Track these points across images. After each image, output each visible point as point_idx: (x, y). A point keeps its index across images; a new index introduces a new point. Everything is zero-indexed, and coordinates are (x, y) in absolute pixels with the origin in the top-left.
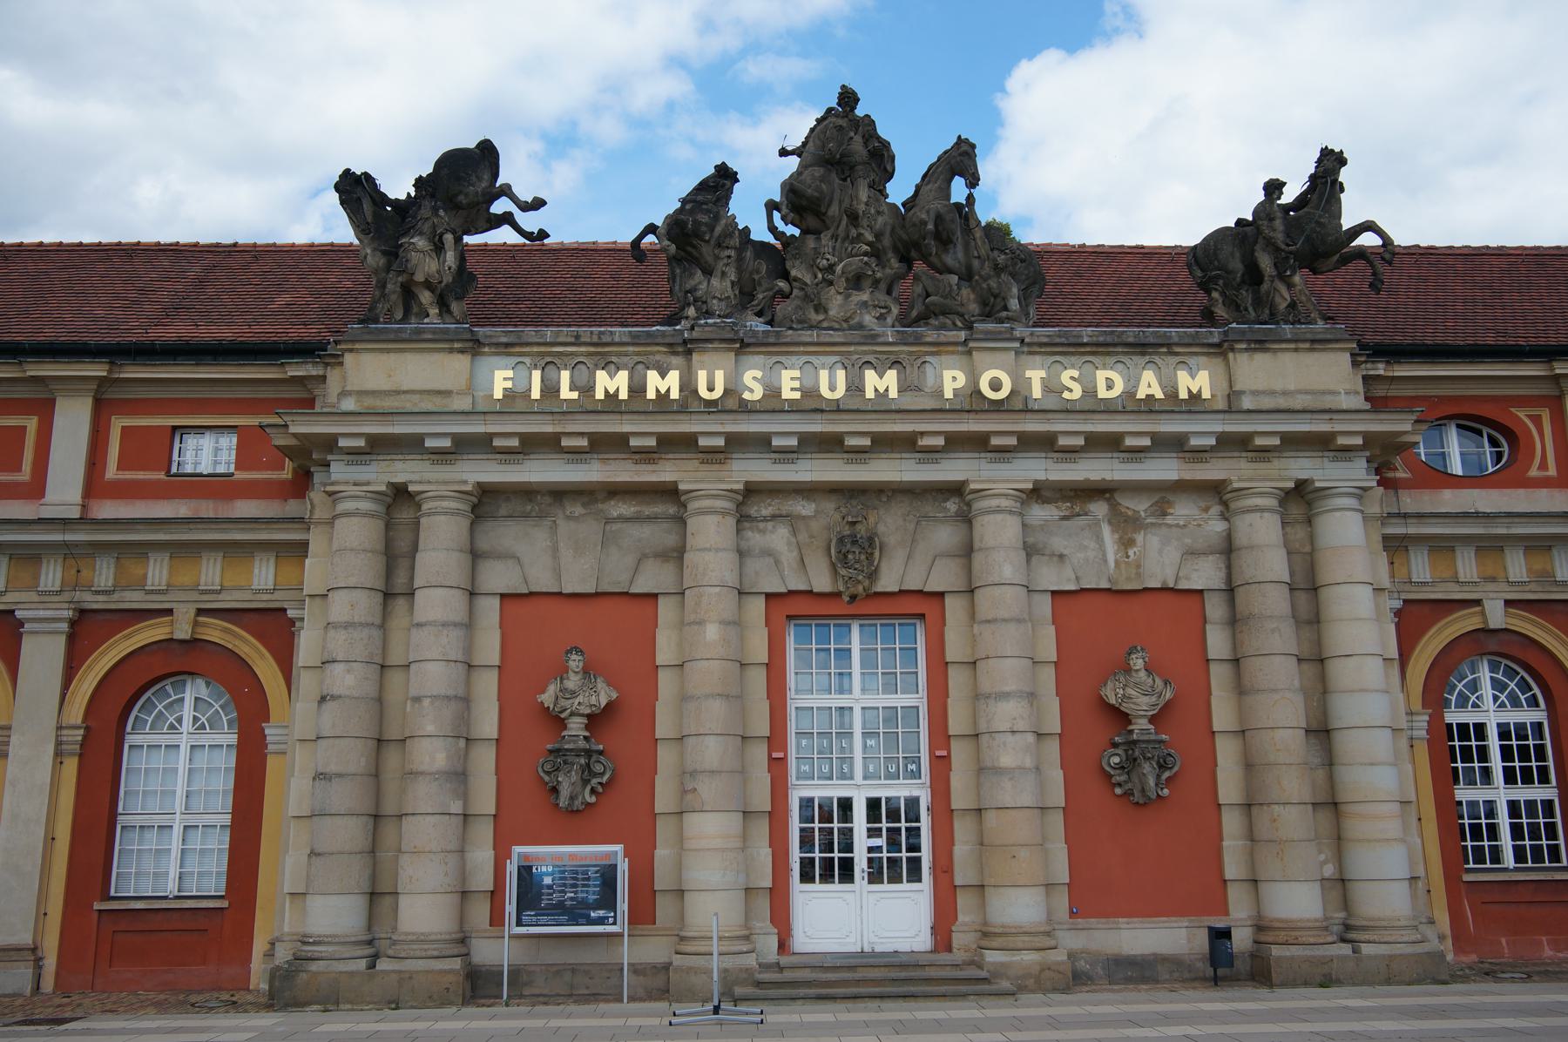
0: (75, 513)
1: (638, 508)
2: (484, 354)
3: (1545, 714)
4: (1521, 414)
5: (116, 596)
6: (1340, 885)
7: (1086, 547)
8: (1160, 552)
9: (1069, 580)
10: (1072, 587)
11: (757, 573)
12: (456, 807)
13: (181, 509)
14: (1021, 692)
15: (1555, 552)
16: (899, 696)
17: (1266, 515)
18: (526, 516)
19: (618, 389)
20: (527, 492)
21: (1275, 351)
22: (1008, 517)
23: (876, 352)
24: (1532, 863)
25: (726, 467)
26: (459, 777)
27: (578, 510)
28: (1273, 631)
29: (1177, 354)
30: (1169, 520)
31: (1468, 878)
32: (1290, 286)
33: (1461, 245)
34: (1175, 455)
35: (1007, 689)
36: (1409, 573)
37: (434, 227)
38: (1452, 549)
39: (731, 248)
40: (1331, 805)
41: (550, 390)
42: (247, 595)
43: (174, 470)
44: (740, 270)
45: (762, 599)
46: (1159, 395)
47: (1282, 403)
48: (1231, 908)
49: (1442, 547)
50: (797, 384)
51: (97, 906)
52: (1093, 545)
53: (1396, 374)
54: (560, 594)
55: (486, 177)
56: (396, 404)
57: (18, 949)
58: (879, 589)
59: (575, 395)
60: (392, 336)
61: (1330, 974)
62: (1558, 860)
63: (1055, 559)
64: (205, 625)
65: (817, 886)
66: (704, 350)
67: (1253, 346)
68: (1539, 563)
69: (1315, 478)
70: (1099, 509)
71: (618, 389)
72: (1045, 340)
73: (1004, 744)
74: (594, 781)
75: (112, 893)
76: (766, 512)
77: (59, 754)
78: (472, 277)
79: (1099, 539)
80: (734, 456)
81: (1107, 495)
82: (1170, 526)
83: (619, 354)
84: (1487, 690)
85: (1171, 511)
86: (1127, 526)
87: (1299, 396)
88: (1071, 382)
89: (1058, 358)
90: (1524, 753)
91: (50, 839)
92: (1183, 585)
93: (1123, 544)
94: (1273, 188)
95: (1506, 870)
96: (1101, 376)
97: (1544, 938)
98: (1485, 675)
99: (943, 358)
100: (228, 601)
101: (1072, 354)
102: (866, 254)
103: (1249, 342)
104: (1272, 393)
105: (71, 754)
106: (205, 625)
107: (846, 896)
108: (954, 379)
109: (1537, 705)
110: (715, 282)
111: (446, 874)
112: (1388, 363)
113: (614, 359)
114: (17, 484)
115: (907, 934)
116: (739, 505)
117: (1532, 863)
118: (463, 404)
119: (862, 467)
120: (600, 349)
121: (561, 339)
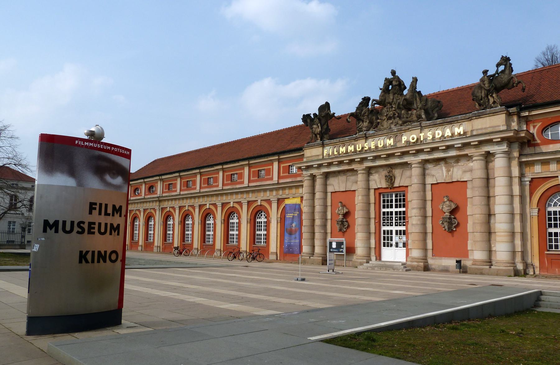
5: (283, 196)
7: (439, 173)
9: (435, 181)
10: (435, 183)
11: (372, 184)
16: (389, 209)
19: (460, 132)
24: (555, 249)
25: (363, 164)
33: (150, 162)
34: (454, 149)
43: (290, 173)
45: (373, 190)
50: (374, 145)
52: (441, 172)
54: (340, 191)
58: (395, 186)
59: (337, 153)
60: (310, 146)
61: (482, 272)
63: (432, 176)
65: (386, 248)
69: (490, 150)
70: (442, 164)
71: (460, 132)
72: (428, 125)
79: (442, 170)
81: (444, 160)
85: (460, 162)
88: (438, 133)
89: (438, 127)
91: (277, 236)
94: (485, 72)
96: (437, 132)
101: (434, 127)
104: (481, 129)
108: (404, 138)
110: (365, 124)
114: (270, 178)
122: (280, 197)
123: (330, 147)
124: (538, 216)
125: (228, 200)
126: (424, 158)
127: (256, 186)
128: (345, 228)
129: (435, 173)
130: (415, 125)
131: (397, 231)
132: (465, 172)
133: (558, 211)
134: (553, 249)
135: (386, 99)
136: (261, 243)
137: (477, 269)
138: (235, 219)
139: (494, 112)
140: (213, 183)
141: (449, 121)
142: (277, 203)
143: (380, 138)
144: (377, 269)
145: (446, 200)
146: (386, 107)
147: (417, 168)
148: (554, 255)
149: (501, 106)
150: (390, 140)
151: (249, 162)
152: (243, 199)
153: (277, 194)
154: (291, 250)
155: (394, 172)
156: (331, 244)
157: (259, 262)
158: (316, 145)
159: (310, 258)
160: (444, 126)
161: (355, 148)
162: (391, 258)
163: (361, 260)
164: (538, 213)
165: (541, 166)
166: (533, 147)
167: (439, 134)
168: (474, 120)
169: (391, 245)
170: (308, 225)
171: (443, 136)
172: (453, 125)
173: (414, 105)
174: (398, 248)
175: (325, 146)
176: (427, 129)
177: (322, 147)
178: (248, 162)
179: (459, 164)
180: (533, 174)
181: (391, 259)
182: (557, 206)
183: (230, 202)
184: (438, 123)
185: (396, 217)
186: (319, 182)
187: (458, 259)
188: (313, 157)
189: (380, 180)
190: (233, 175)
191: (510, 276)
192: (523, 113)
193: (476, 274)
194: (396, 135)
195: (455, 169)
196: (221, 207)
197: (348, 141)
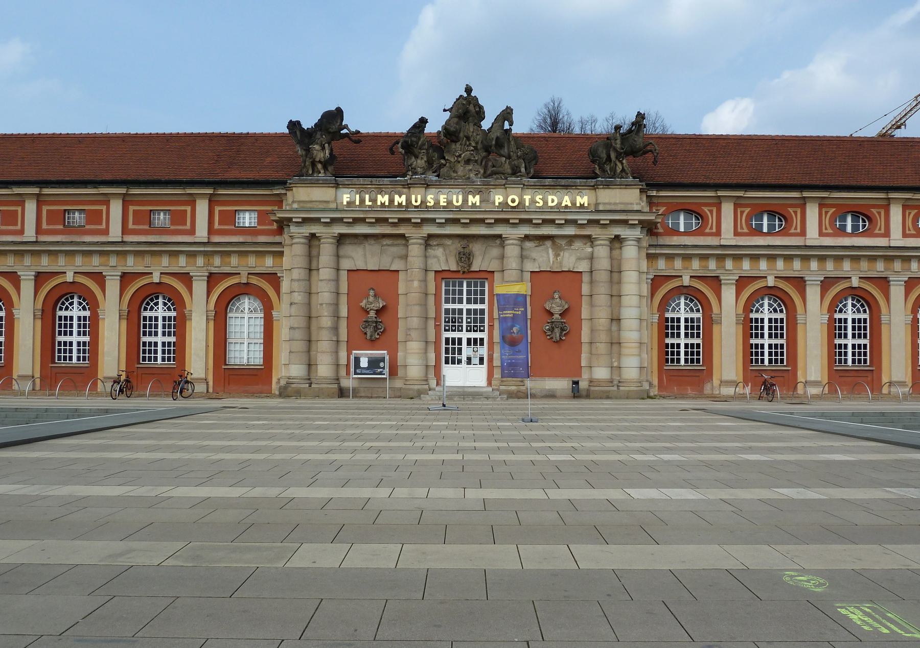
0: (34, 240)
5: (222, 268)
9: (536, 268)
11: (432, 264)
26: (335, 329)
31: (665, 368)
41: (362, 201)
43: (237, 225)
46: (570, 205)
50: (445, 200)
52: (545, 255)
54: (367, 270)
59: (370, 203)
63: (532, 260)
64: (251, 278)
68: (704, 263)
70: (548, 243)
72: (533, 184)
77: (34, 318)
79: (548, 253)
85: (573, 244)
88: (553, 199)
90: (692, 328)
91: (207, 346)
92: (576, 270)
95: (681, 365)
96: (550, 198)
99: (497, 190)
100: (257, 270)
104: (610, 204)
105: (212, 319)
106: (251, 278)
108: (499, 199)
110: (419, 161)
112: (657, 191)
118: (333, 206)
123: (351, 190)
124: (214, 320)
125: (58, 268)
126: (527, 233)
127: (97, 243)
128: (378, 334)
129: (536, 256)
130: (513, 181)
131: (469, 340)
132: (579, 259)
133: (862, 318)
134: (146, 361)
135: (462, 130)
137: (602, 391)
138: (160, 310)
139: (626, 183)
140: (86, 225)
141: (563, 184)
142: (33, 281)
143: (452, 190)
144: (458, 399)
145: (556, 296)
146: (459, 143)
147: (516, 246)
148: (864, 371)
149: (634, 178)
150: (383, 198)
151: (127, 191)
152: (108, 268)
153: (208, 264)
154: (512, 371)
155: (472, 247)
156: (357, 360)
157: (185, 398)
158: (321, 182)
159: (310, 386)
160: (557, 190)
161: (408, 200)
162: (481, 382)
163: (419, 387)
164: (42, 316)
165: (699, 261)
166: (655, 237)
167: (553, 201)
168: (599, 190)
169: (460, 362)
170: (301, 326)
171: (560, 203)
172: (568, 190)
173: (504, 150)
174: (472, 366)
175: (340, 188)
176: (530, 190)
177: (335, 189)
178: (126, 190)
179: (572, 247)
180: (656, 271)
181: (481, 383)
183: (65, 273)
184: (547, 184)
185: (467, 318)
186: (326, 250)
188: (314, 203)
189: (446, 257)
190: (68, 212)
191: (643, 399)
192: (650, 192)
193: (601, 398)
194: (479, 190)
195: (567, 254)
196: (33, 282)
197: (390, 186)
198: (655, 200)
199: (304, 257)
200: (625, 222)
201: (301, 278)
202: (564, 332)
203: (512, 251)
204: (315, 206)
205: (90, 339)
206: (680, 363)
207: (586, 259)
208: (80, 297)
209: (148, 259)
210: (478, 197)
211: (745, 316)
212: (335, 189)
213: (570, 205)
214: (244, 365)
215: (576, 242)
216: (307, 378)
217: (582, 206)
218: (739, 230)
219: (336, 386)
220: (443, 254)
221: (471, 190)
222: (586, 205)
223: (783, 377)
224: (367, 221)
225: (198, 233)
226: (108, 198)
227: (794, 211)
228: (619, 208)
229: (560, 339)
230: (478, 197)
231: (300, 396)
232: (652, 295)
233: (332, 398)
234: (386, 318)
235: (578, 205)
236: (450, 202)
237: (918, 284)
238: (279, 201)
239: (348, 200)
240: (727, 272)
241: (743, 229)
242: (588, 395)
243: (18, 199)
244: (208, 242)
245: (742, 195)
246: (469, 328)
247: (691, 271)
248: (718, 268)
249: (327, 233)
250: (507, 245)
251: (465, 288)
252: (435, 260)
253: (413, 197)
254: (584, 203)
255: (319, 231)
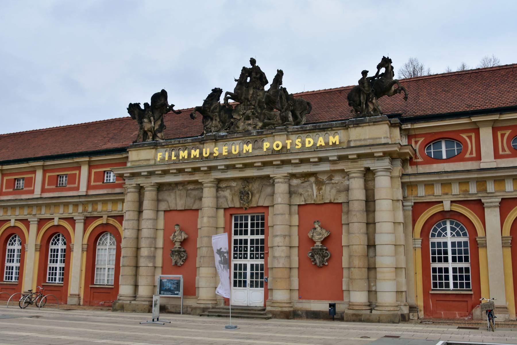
0: (85, 194)
1: (194, 186)
2: (158, 148)
3: (468, 238)
4: (464, 136)
6: (372, 293)
8: (330, 192)
9: (303, 201)
11: (221, 202)
12: (151, 265)
13: (110, 191)
14: (282, 235)
15: (470, 184)
17: (356, 179)
18: (169, 190)
20: (169, 184)
21: (363, 126)
22: (281, 184)
23: (250, 138)
25: (210, 175)
26: (153, 257)
27: (181, 188)
28: (354, 215)
29: (334, 130)
30: (333, 181)
31: (431, 292)
32: (373, 104)
35: (277, 234)
36: (418, 193)
37: (149, 116)
38: (433, 185)
39: (216, 112)
40: (371, 268)
41: (170, 157)
42: (117, 212)
43: (105, 181)
44: (220, 118)
46: (323, 144)
47: (363, 143)
48: (344, 298)
49: (429, 185)
50: (226, 150)
51: (90, 286)
52: (310, 190)
53: (415, 127)
54: (176, 210)
55: (163, 100)
56: (139, 164)
57: (76, 295)
58: (252, 206)
59: (175, 158)
62: (449, 287)
63: (299, 195)
64: (109, 220)
65: (237, 288)
66: (207, 143)
67: (355, 126)
68: (464, 188)
70: (312, 179)
72: (296, 130)
73: (276, 249)
74: (182, 259)
75: (95, 283)
76: (224, 186)
77: (83, 251)
78: (164, 126)
80: (212, 171)
81: (315, 175)
82: (333, 183)
83: (189, 146)
84: (449, 231)
85: (333, 179)
86: (320, 184)
87: (369, 140)
88: (309, 142)
89: (300, 135)
92: (336, 201)
93: (319, 190)
94: (365, 73)
95: (449, 290)
96: (307, 140)
97: (457, 313)
98: (448, 226)
99: (269, 138)
100: (114, 214)
102: (253, 109)
103: (354, 124)
104: (360, 140)
105: (85, 251)
106: (109, 220)
107: (245, 291)
108: (266, 145)
109: (467, 236)
110: (214, 122)
111: (147, 281)
112: (411, 124)
113: (188, 147)
114: (75, 187)
115: (242, 301)
116: (217, 184)
117: (460, 288)
118: (152, 162)
119: (244, 172)
120: (184, 145)
121: (175, 143)
122: (88, 215)
125: (7, 217)
126: (290, 172)
136: (55, 280)
138: (60, 245)
139: (374, 120)
151: (44, 163)
152: (31, 216)
153: (85, 210)
161: (201, 154)
166: (415, 166)
167: (309, 142)
171: (315, 144)
176: (294, 136)
180: (416, 198)
182: (441, 237)
185: (251, 247)
186: (149, 195)
187: (332, 302)
188: (140, 162)
191: (394, 323)
195: (328, 188)
198: (413, 133)
199: (151, 201)
200: (371, 156)
201: (130, 219)
202: (326, 259)
203: (281, 188)
204: (141, 164)
205: (20, 265)
206: (449, 288)
207: (345, 191)
208: (63, 236)
209: (53, 209)
210: (250, 146)
211: (512, 238)
212: (214, 143)
213: (323, 144)
214: (104, 285)
215: (335, 177)
216: (289, 301)
217: (334, 144)
218: (501, 152)
219: (147, 303)
220: (230, 194)
221: (249, 140)
222: (337, 143)
223: (60, 291)
224: (292, 162)
225: (81, 189)
226: (35, 169)
227: (468, 136)
228: (368, 143)
229: (323, 264)
230: (250, 146)
231: (123, 310)
232: (414, 222)
233: (144, 312)
234: (189, 248)
235: (331, 144)
236: (229, 152)
237: (516, 206)
238: (124, 163)
239: (161, 157)
240: (490, 195)
241: (505, 151)
242: (341, 319)
243: (75, 165)
244: (86, 195)
245: (498, 118)
246: (246, 256)
247: (451, 196)
248: (478, 192)
249: (149, 183)
250: (146, 191)
251: (249, 222)
252: (225, 199)
253: (204, 150)
254: (335, 142)
255: (142, 182)
